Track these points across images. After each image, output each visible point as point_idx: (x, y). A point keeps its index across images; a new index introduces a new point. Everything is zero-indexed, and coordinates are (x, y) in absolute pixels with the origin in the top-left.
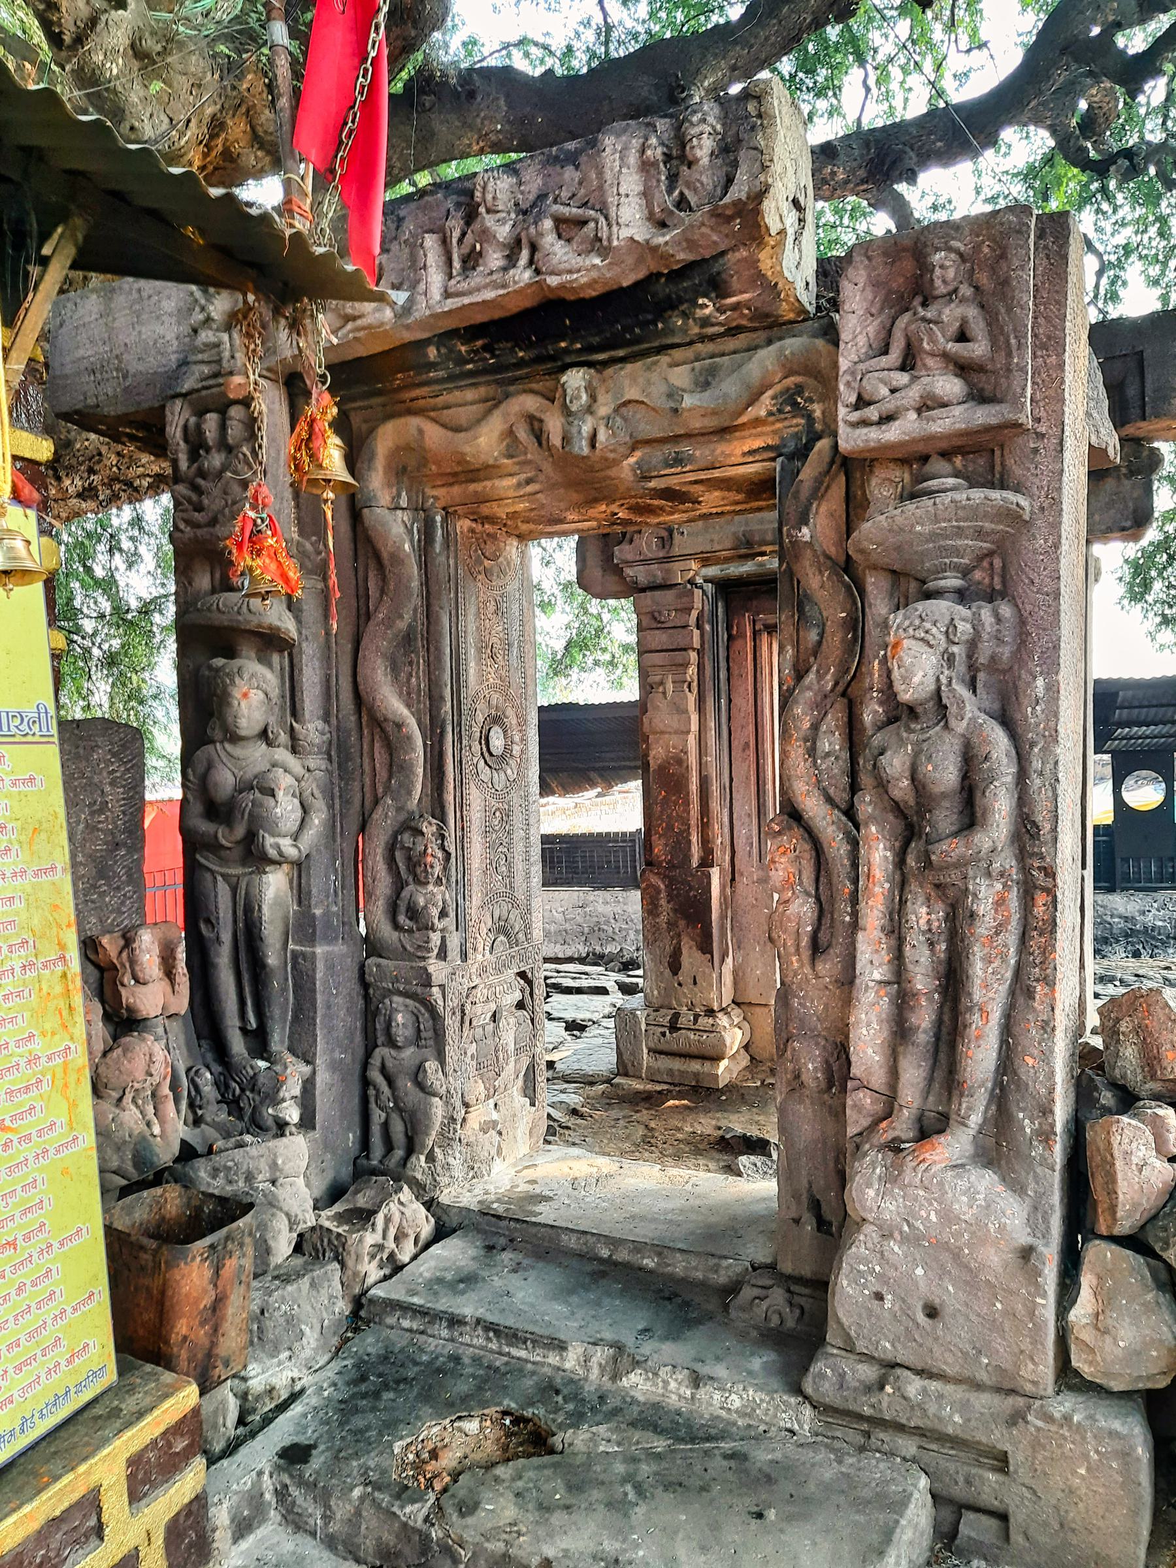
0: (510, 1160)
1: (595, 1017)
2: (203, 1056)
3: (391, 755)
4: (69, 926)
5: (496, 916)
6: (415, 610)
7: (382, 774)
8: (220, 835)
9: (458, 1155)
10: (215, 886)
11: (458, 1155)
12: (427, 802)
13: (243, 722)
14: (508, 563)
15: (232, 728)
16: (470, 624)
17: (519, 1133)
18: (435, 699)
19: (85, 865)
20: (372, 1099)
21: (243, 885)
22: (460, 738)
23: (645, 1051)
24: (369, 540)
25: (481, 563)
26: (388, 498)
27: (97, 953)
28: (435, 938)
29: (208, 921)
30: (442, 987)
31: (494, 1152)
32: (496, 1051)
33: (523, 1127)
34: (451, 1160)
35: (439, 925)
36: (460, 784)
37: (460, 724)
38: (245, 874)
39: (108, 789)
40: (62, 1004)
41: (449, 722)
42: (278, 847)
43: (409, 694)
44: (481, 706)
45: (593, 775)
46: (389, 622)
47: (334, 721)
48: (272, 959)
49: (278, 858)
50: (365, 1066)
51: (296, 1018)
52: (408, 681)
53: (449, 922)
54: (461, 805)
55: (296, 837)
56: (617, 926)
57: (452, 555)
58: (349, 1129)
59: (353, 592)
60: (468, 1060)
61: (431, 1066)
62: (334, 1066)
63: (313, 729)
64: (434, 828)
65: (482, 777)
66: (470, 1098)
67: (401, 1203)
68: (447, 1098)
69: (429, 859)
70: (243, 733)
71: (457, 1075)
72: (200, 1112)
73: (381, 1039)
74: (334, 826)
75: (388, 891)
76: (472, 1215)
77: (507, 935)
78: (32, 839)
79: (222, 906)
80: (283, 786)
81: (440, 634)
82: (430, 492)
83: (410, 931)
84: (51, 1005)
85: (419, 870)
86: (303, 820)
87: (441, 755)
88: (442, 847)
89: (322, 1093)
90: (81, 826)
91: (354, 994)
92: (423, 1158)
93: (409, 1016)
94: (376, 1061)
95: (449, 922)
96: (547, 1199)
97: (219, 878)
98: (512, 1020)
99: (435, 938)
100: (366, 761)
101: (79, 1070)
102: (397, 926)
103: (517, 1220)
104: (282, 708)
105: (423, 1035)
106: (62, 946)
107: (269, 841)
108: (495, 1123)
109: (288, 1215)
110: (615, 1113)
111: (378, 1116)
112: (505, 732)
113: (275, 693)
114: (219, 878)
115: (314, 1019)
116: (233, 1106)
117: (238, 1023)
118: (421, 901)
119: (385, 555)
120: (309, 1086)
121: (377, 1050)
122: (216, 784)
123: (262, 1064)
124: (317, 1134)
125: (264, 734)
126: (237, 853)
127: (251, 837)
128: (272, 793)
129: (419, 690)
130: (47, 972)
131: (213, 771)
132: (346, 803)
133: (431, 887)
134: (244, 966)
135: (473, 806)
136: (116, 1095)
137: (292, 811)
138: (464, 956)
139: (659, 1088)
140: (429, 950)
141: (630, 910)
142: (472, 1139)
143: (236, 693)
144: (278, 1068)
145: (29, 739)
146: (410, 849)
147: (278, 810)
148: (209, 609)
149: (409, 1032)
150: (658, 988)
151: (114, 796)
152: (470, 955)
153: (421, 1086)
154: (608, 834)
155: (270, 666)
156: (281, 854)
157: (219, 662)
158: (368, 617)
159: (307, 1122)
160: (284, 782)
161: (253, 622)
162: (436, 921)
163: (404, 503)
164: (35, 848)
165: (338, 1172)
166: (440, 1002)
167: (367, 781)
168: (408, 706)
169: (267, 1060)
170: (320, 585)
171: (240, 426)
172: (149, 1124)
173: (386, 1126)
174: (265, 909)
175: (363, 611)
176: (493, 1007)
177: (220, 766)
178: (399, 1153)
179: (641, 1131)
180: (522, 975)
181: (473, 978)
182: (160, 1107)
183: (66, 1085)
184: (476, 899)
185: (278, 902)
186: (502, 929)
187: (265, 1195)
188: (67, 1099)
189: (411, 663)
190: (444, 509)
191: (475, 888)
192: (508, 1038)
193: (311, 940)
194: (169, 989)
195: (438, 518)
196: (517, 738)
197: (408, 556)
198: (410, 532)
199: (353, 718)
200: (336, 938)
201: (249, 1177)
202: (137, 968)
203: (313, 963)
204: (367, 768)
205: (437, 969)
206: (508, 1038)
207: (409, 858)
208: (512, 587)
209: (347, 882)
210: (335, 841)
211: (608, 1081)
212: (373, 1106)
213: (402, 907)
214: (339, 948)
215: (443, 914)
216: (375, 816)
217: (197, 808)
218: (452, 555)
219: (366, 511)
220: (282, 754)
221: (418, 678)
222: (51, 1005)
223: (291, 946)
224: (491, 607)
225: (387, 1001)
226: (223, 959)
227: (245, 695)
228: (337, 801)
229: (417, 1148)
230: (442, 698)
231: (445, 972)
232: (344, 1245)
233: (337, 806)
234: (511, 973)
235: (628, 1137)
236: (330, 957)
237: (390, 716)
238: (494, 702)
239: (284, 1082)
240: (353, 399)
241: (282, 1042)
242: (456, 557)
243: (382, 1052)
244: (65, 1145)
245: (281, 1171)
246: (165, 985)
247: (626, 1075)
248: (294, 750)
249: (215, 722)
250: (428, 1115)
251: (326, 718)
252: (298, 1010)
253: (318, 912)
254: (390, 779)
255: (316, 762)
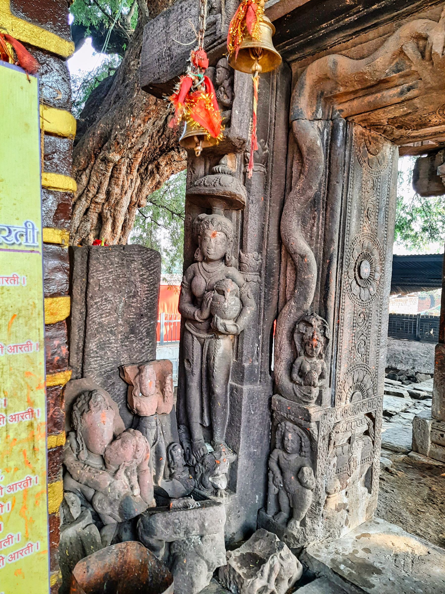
0: (353, 526)
1: (398, 410)
2: (180, 436)
3: (296, 274)
4: (39, 387)
5: (355, 379)
6: (320, 184)
7: (291, 286)
8: (196, 315)
9: (320, 524)
10: (193, 343)
11: (320, 524)
12: (317, 305)
13: (212, 251)
14: (384, 158)
15: (206, 254)
16: (355, 194)
17: (360, 511)
18: (327, 241)
19: (123, 326)
20: (271, 479)
21: (207, 344)
22: (342, 267)
23: (430, 442)
24: (296, 141)
25: (366, 156)
26: (310, 114)
27: (124, 376)
28: (315, 392)
29: (188, 361)
30: (318, 423)
31: (343, 522)
32: (349, 461)
33: (363, 506)
34: (316, 526)
35: (318, 383)
36: (339, 296)
37: (342, 258)
38: (208, 338)
39: (138, 284)
40: (27, 447)
41: (335, 256)
42: (224, 325)
43: (311, 237)
44: (357, 247)
45: (398, 287)
46: (303, 191)
47: (264, 253)
48: (218, 390)
49: (224, 332)
50: (268, 457)
51: (230, 425)
52: (312, 229)
53: (325, 382)
54: (339, 309)
55: (236, 320)
56: (404, 357)
57: (348, 148)
58: (256, 493)
59: (283, 175)
60: (331, 467)
61: (307, 470)
62: (250, 456)
63: (251, 257)
64: (320, 323)
65: (354, 292)
66: (330, 490)
67: (281, 557)
68: (316, 491)
69: (315, 342)
70: (211, 257)
71: (322, 476)
72: (173, 471)
73: (278, 445)
74: (260, 315)
75: (288, 357)
76: (327, 570)
77: (362, 390)
78: (11, 323)
79: (195, 354)
80: (230, 290)
81: (336, 199)
82: (337, 107)
83: (300, 385)
84: (16, 448)
85: (308, 348)
86: (241, 310)
87: (328, 276)
88: (324, 335)
89: (242, 472)
90: (122, 304)
91: (265, 414)
92: (298, 523)
93: (296, 436)
94: (274, 457)
95: (325, 382)
96: (379, 572)
97: (195, 338)
98: (361, 443)
99: (315, 392)
100: (282, 277)
101: (38, 495)
102: (292, 380)
103: (357, 587)
104: (235, 244)
105: (304, 449)
106: (31, 403)
107: (220, 321)
108: (345, 505)
109: (207, 562)
110: (410, 476)
111: (273, 490)
112: (371, 264)
113: (231, 235)
114: (195, 338)
115: (239, 427)
116: (192, 468)
117: (199, 421)
118: (308, 368)
119: (304, 149)
120: (234, 466)
121: (276, 450)
122: (196, 286)
123: (209, 448)
124: (236, 496)
125: (223, 259)
126: (204, 326)
127: (211, 317)
128: (223, 293)
129: (318, 235)
130: (15, 423)
131: (195, 278)
132: (267, 301)
133: (315, 359)
134: (204, 389)
135: (346, 310)
136: (114, 468)
137: (234, 305)
138: (333, 403)
139: (437, 464)
140: (310, 398)
141: (411, 350)
142: (330, 515)
143: (209, 233)
144: (216, 454)
145: (16, 247)
146: (303, 334)
147: (226, 304)
148: (200, 185)
149: (295, 446)
150: (441, 410)
151: (142, 289)
152: (337, 403)
153: (300, 482)
154: (403, 315)
155: (231, 219)
156: (226, 330)
157: (203, 216)
158: (291, 189)
159: (232, 487)
160: (231, 287)
161: (219, 190)
162: (316, 381)
163: (319, 116)
164: (13, 329)
165: (247, 516)
166: (316, 432)
167: (282, 289)
168: (310, 245)
169: (213, 446)
170: (263, 170)
171: (224, 71)
172: (132, 488)
173: (278, 495)
174: (217, 359)
175: (288, 187)
176: (349, 434)
177: (199, 276)
178: (285, 515)
179: (426, 491)
180: (369, 415)
181: (337, 417)
182: (141, 476)
183: (25, 507)
184: (344, 367)
185: (224, 356)
186: (359, 387)
187: (194, 547)
188: (25, 517)
189: (314, 218)
190: (346, 118)
191: (343, 361)
192: (357, 454)
193: (241, 381)
194: (161, 399)
195: (341, 124)
196: (378, 268)
197: (319, 148)
198: (322, 134)
199: (276, 252)
200: (256, 381)
201: (187, 532)
202: (143, 387)
203: (241, 395)
204: (282, 281)
205: (315, 411)
206: (357, 454)
207: (302, 340)
208: (385, 172)
209: (265, 349)
210: (259, 323)
211: (406, 453)
212: (271, 483)
213: (296, 370)
214: (258, 387)
215: (322, 377)
216: (283, 311)
217: (187, 298)
218: (348, 148)
219: (295, 122)
220: (233, 271)
221: (318, 227)
222: (16, 448)
223: (230, 382)
224: (370, 184)
225: (283, 424)
226: (194, 383)
227: (214, 235)
228: (262, 300)
229: (295, 516)
230: (332, 240)
231: (320, 414)
232: (242, 584)
233: (262, 304)
234: (361, 415)
235: (419, 494)
236: (253, 391)
237: (298, 251)
238: (366, 245)
239: (218, 465)
240: (292, 52)
241: (221, 437)
242: (350, 151)
243: (278, 452)
244: (21, 553)
245: (207, 530)
246: (159, 397)
247: (417, 451)
248: (240, 269)
249: (198, 250)
250: (302, 500)
251: (260, 250)
252: (232, 419)
253: (246, 365)
254: (295, 289)
255: (253, 276)
